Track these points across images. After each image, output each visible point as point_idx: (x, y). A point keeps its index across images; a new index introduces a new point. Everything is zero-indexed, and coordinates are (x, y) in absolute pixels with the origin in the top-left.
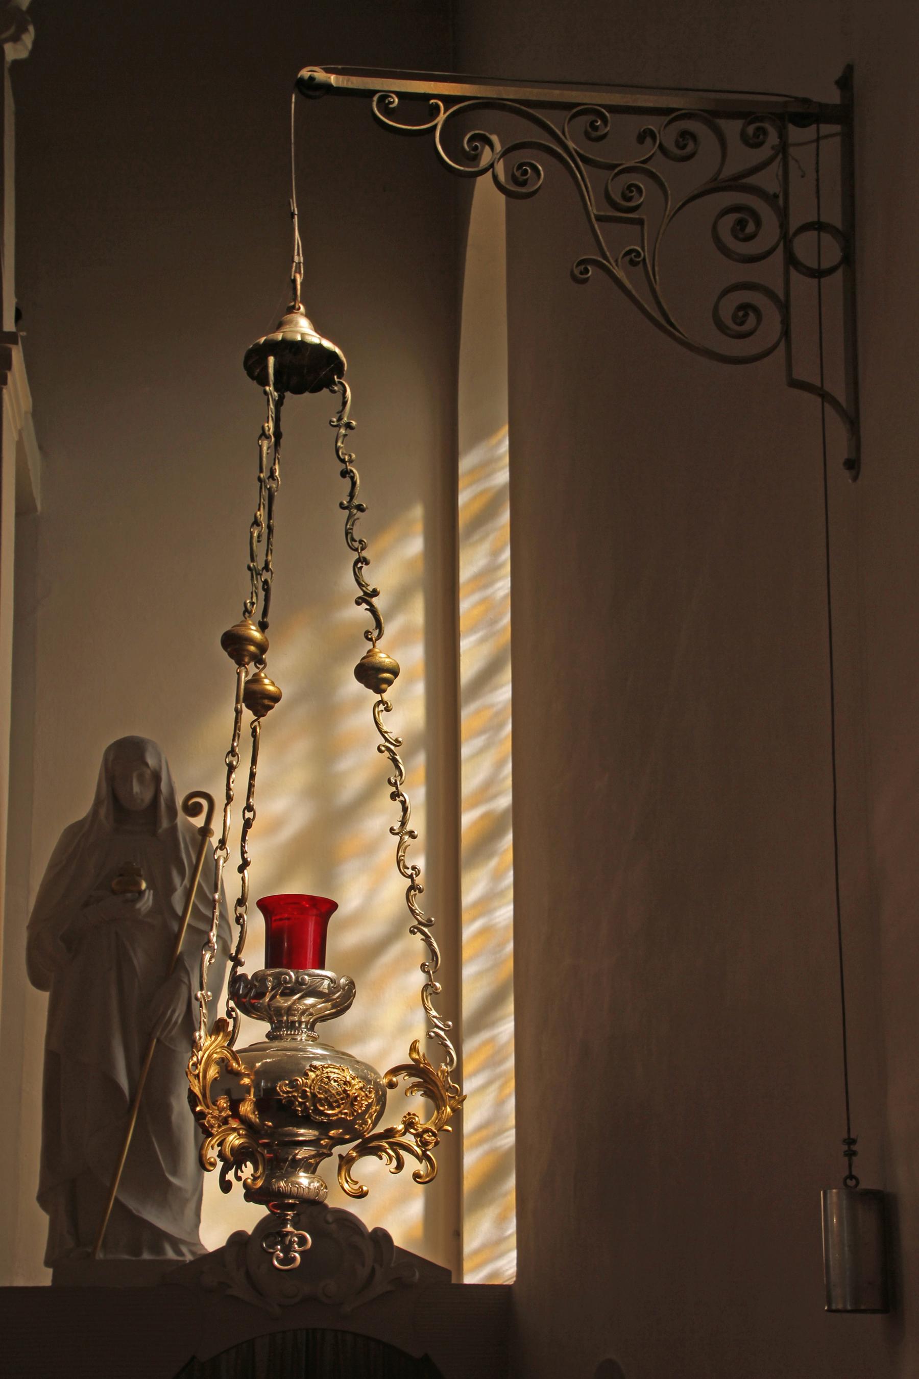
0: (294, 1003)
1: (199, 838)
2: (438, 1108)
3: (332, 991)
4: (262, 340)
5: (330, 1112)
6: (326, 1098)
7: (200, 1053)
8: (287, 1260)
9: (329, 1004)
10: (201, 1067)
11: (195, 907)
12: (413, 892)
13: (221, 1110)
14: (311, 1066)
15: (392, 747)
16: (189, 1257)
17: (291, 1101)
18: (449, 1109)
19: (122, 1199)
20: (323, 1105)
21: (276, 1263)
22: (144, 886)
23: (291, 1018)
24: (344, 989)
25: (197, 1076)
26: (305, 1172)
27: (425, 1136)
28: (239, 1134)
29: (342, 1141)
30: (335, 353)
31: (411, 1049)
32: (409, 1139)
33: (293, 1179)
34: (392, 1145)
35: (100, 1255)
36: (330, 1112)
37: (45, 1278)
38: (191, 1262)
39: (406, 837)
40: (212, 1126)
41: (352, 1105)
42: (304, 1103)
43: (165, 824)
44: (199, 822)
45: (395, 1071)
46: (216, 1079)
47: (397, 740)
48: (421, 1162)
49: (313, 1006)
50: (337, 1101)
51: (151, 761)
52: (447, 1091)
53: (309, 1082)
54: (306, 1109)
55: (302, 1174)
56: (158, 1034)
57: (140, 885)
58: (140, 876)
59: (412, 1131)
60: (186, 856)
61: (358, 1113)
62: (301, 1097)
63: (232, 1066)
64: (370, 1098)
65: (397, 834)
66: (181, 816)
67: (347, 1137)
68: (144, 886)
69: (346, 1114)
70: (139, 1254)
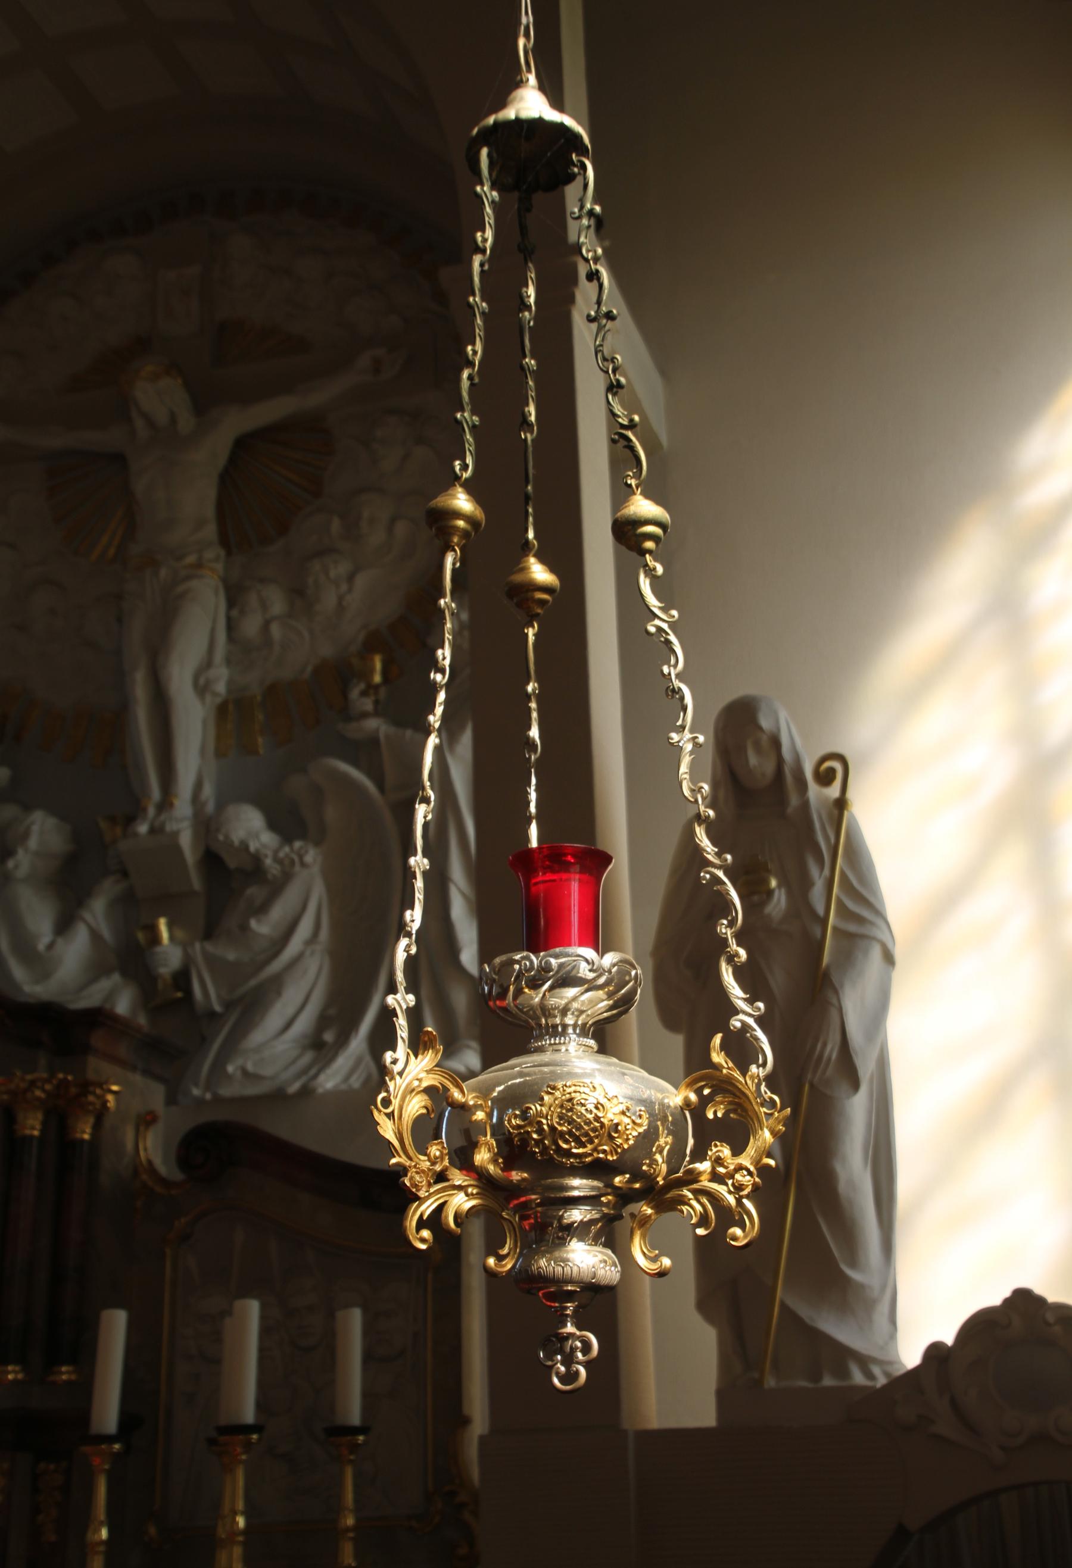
1: (836, 812)
4: (475, 131)
5: (581, 1151)
6: (570, 1132)
8: (570, 1377)
11: (839, 902)
16: (882, 1381)
17: (525, 1138)
19: (790, 1302)
21: (556, 1381)
22: (774, 883)
24: (610, 972)
26: (581, 1240)
27: (738, 1176)
28: (467, 1195)
30: (561, 126)
33: (557, 1254)
35: (770, 1382)
38: (884, 1387)
43: (794, 801)
44: (834, 791)
51: (765, 723)
52: (762, 1105)
54: (545, 1150)
56: (809, 1076)
57: (768, 883)
58: (768, 871)
62: (536, 1132)
64: (640, 1125)
66: (814, 790)
68: (774, 883)
69: (604, 1151)
70: (816, 1377)
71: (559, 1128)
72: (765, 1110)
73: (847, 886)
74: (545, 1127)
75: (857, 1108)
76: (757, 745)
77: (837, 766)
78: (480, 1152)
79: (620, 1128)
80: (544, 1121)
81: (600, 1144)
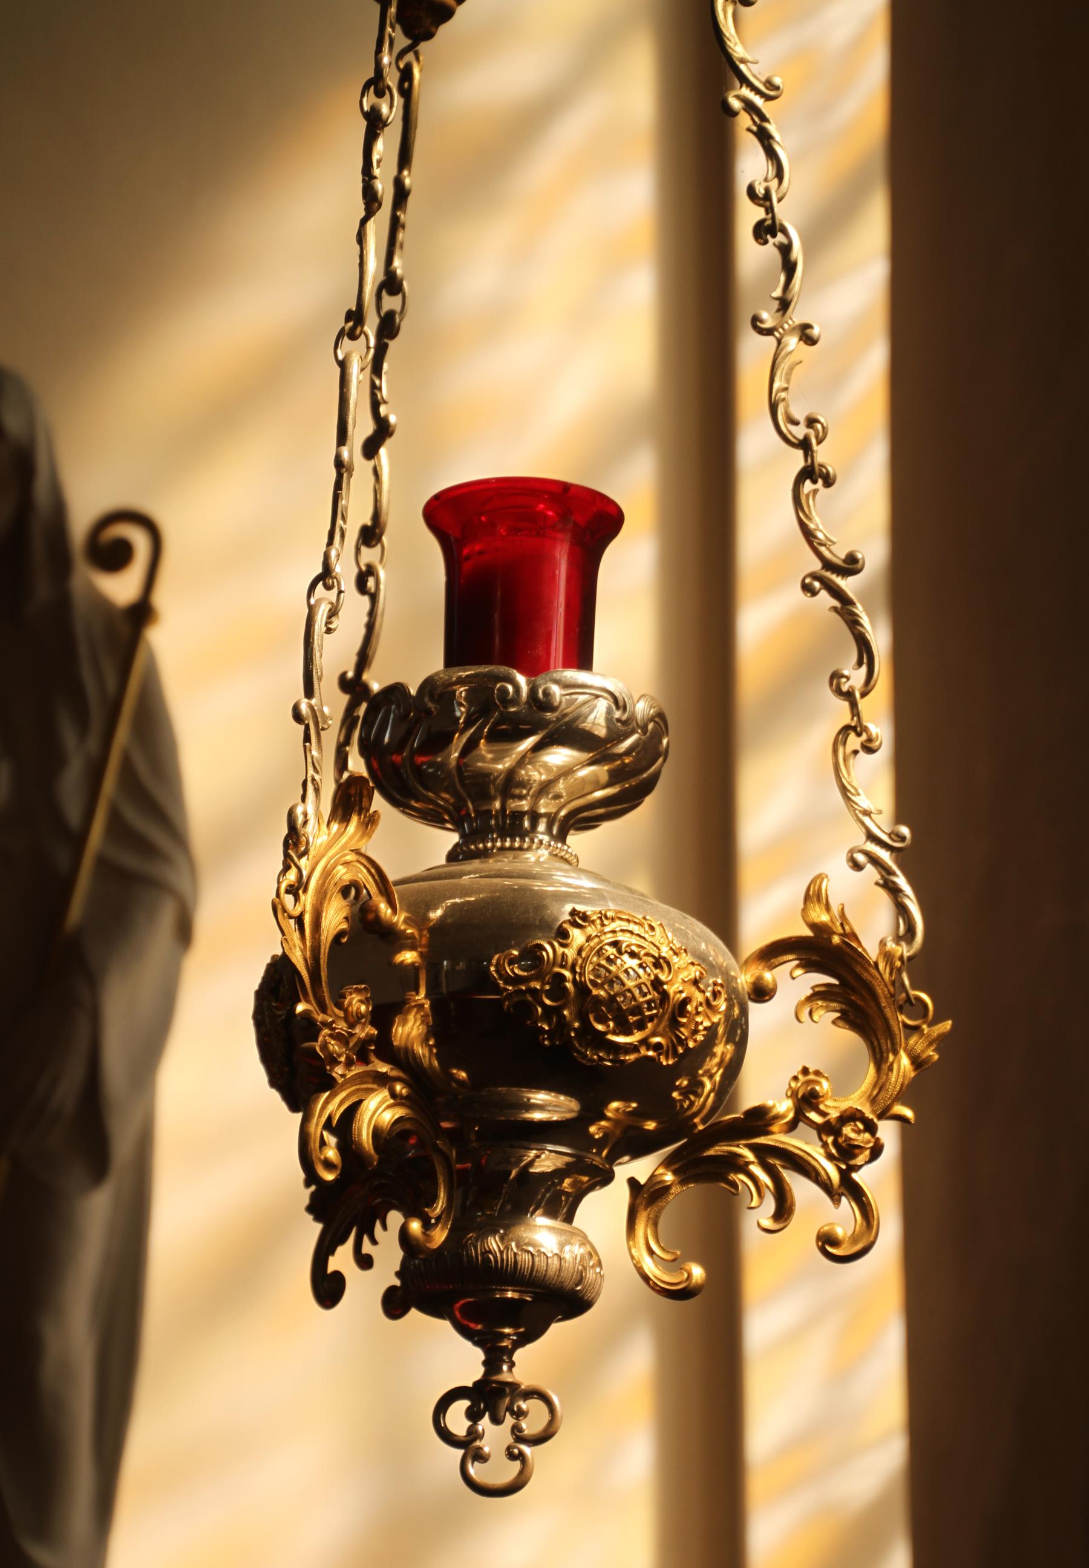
0: (521, 762)
2: (879, 1059)
3: (616, 735)
5: (621, 1039)
6: (612, 999)
7: (303, 863)
9: (601, 771)
10: (308, 899)
12: (808, 486)
13: (353, 1020)
14: (574, 913)
15: (758, 101)
17: (524, 1005)
18: (905, 1061)
20: (603, 1020)
23: (513, 805)
24: (644, 729)
25: (300, 920)
27: (847, 1130)
28: (393, 1095)
29: (640, 1146)
31: (807, 898)
32: (806, 1144)
34: (763, 1153)
36: (621, 1039)
39: (792, 342)
40: (334, 1062)
41: (675, 1024)
42: (558, 1010)
43: (43, 591)
45: (772, 953)
46: (340, 934)
47: (769, 84)
48: (836, 1201)
49: (567, 772)
50: (637, 1010)
52: (901, 1009)
53: (571, 953)
54: (563, 1025)
55: (541, 1220)
59: (813, 1116)
61: (687, 1049)
63: (376, 911)
65: (769, 332)
67: (651, 1125)
69: (657, 1047)
71: (595, 992)
72: (902, 1018)
73: (129, 778)
74: (569, 985)
75: (96, 1211)
77: (140, 540)
78: (405, 1022)
79: (689, 1008)
80: (567, 974)
81: (654, 1034)
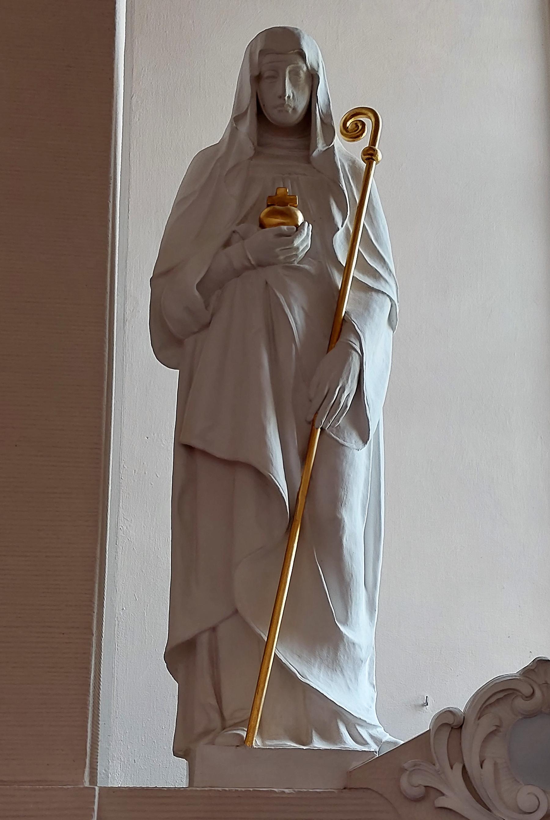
19: (355, 276)
22: (301, 219)
35: (257, 742)
37: (174, 774)
43: (321, 146)
57: (297, 219)
60: (350, 188)
68: (301, 219)
70: (309, 741)
76: (295, 73)
